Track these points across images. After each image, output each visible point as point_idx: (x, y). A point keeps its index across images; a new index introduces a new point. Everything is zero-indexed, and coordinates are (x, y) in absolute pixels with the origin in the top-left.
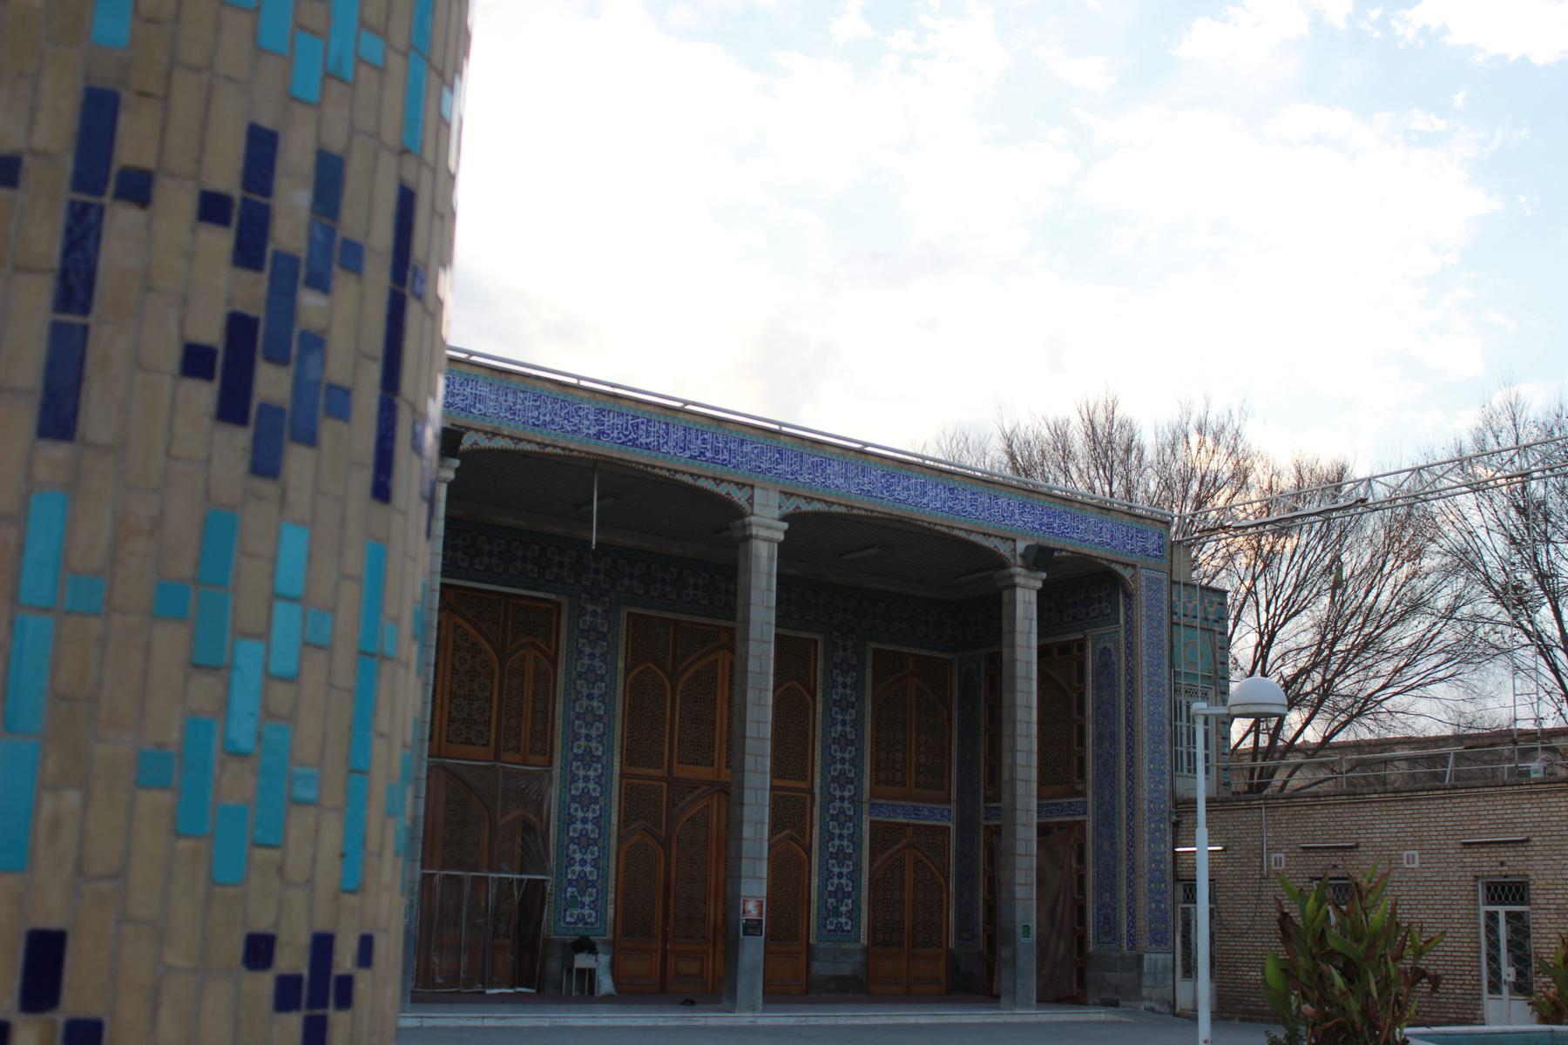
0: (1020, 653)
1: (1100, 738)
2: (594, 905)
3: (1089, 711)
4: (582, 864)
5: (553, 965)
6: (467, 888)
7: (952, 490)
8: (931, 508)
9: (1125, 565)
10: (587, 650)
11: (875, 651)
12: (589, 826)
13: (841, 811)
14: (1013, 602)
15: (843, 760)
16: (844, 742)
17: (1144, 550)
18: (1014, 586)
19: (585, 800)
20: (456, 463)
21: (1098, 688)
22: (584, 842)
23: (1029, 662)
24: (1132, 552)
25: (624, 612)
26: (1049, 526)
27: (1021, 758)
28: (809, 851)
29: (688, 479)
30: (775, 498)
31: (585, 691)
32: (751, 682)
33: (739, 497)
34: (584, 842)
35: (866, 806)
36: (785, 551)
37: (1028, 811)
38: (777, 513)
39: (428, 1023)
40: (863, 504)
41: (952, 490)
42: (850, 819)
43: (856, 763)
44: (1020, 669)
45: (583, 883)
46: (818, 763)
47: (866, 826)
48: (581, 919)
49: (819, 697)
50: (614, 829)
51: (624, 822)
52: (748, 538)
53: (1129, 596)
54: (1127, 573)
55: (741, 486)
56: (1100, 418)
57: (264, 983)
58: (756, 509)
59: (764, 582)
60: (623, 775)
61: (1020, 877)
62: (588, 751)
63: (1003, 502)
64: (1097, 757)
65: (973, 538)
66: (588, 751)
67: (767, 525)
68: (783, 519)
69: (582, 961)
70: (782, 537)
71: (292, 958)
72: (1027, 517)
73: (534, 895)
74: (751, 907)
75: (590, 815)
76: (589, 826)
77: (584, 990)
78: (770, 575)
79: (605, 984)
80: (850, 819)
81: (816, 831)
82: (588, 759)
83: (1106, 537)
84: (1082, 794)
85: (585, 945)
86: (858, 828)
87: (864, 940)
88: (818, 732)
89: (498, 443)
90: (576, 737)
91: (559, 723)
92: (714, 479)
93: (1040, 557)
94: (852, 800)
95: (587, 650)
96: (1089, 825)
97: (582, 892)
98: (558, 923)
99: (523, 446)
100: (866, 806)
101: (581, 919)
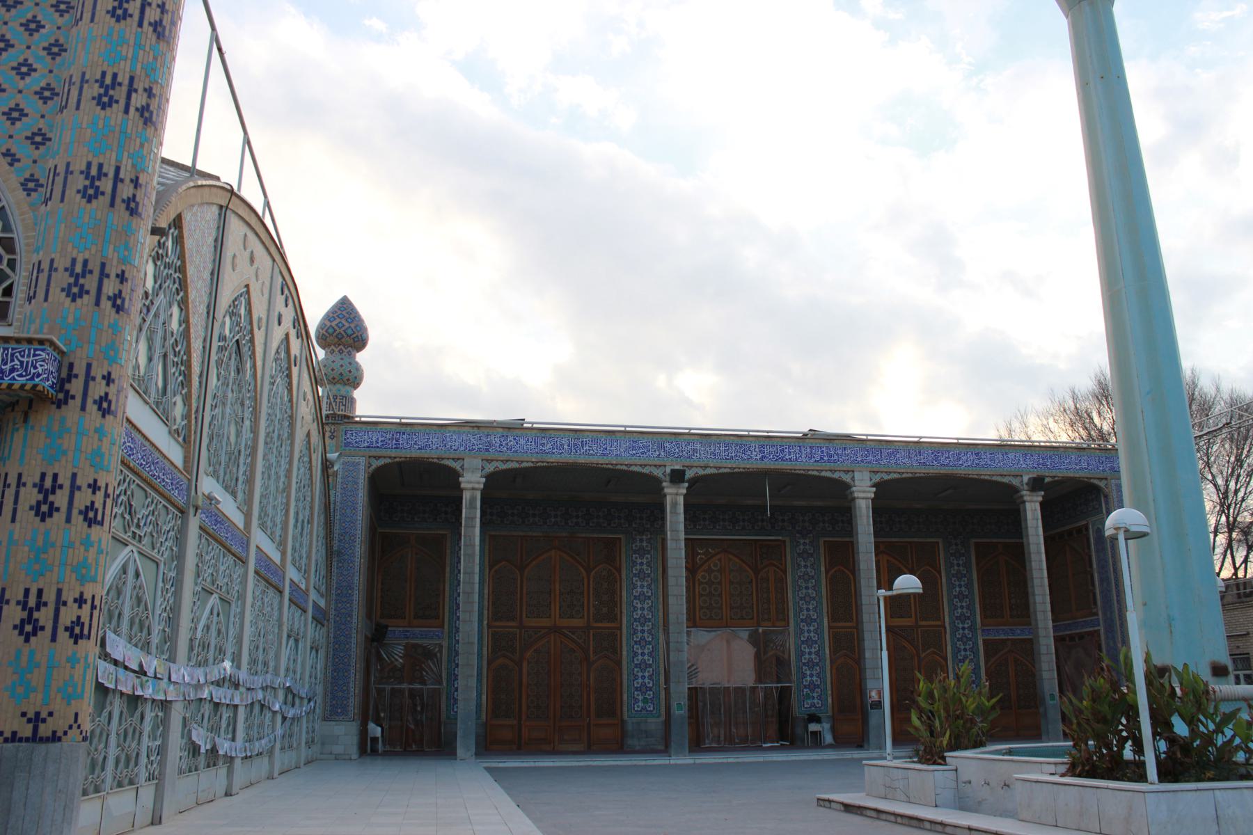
0: (1032, 539)
1: (1101, 580)
2: (820, 697)
3: (1095, 566)
4: (811, 676)
5: (799, 731)
6: (748, 693)
7: (977, 454)
8: (965, 467)
9: (1100, 479)
10: (803, 563)
11: (977, 544)
13: (964, 635)
14: (1025, 510)
15: (962, 607)
16: (961, 597)
18: (1024, 502)
19: (809, 642)
20: (686, 485)
21: (1097, 551)
22: (811, 665)
23: (1038, 544)
24: (1104, 470)
25: (822, 541)
26: (1044, 464)
27: (1038, 599)
28: (946, 659)
29: (815, 473)
30: (867, 475)
31: (804, 585)
32: (862, 575)
33: (846, 478)
34: (811, 665)
35: (979, 632)
37: (1046, 628)
38: (869, 483)
39: (698, 761)
40: (921, 471)
41: (977, 454)
42: (970, 639)
43: (970, 607)
44: (1033, 548)
45: (813, 687)
46: (946, 610)
47: (980, 642)
48: (813, 705)
49: (943, 574)
50: (828, 656)
51: (834, 651)
52: (854, 499)
53: (1106, 496)
54: (1102, 484)
55: (847, 472)
57: (25, 719)
58: (857, 483)
60: (830, 627)
61: (1045, 666)
62: (809, 616)
63: (1011, 456)
64: (1101, 592)
65: (994, 478)
66: (809, 616)
67: (472, 481)
69: (813, 727)
71: (31, 715)
72: (1028, 461)
73: (784, 694)
77: (816, 741)
79: (829, 738)
80: (970, 639)
81: (949, 648)
82: (809, 620)
83: (1084, 465)
84: (1096, 614)
85: (814, 718)
86: (975, 644)
88: (945, 593)
89: (708, 471)
90: (801, 610)
91: (791, 604)
93: (1037, 484)
94: (970, 629)
95: (803, 563)
96: (1102, 631)
97: (812, 691)
98: (800, 707)
99: (722, 471)
100: (979, 632)
101: (813, 705)
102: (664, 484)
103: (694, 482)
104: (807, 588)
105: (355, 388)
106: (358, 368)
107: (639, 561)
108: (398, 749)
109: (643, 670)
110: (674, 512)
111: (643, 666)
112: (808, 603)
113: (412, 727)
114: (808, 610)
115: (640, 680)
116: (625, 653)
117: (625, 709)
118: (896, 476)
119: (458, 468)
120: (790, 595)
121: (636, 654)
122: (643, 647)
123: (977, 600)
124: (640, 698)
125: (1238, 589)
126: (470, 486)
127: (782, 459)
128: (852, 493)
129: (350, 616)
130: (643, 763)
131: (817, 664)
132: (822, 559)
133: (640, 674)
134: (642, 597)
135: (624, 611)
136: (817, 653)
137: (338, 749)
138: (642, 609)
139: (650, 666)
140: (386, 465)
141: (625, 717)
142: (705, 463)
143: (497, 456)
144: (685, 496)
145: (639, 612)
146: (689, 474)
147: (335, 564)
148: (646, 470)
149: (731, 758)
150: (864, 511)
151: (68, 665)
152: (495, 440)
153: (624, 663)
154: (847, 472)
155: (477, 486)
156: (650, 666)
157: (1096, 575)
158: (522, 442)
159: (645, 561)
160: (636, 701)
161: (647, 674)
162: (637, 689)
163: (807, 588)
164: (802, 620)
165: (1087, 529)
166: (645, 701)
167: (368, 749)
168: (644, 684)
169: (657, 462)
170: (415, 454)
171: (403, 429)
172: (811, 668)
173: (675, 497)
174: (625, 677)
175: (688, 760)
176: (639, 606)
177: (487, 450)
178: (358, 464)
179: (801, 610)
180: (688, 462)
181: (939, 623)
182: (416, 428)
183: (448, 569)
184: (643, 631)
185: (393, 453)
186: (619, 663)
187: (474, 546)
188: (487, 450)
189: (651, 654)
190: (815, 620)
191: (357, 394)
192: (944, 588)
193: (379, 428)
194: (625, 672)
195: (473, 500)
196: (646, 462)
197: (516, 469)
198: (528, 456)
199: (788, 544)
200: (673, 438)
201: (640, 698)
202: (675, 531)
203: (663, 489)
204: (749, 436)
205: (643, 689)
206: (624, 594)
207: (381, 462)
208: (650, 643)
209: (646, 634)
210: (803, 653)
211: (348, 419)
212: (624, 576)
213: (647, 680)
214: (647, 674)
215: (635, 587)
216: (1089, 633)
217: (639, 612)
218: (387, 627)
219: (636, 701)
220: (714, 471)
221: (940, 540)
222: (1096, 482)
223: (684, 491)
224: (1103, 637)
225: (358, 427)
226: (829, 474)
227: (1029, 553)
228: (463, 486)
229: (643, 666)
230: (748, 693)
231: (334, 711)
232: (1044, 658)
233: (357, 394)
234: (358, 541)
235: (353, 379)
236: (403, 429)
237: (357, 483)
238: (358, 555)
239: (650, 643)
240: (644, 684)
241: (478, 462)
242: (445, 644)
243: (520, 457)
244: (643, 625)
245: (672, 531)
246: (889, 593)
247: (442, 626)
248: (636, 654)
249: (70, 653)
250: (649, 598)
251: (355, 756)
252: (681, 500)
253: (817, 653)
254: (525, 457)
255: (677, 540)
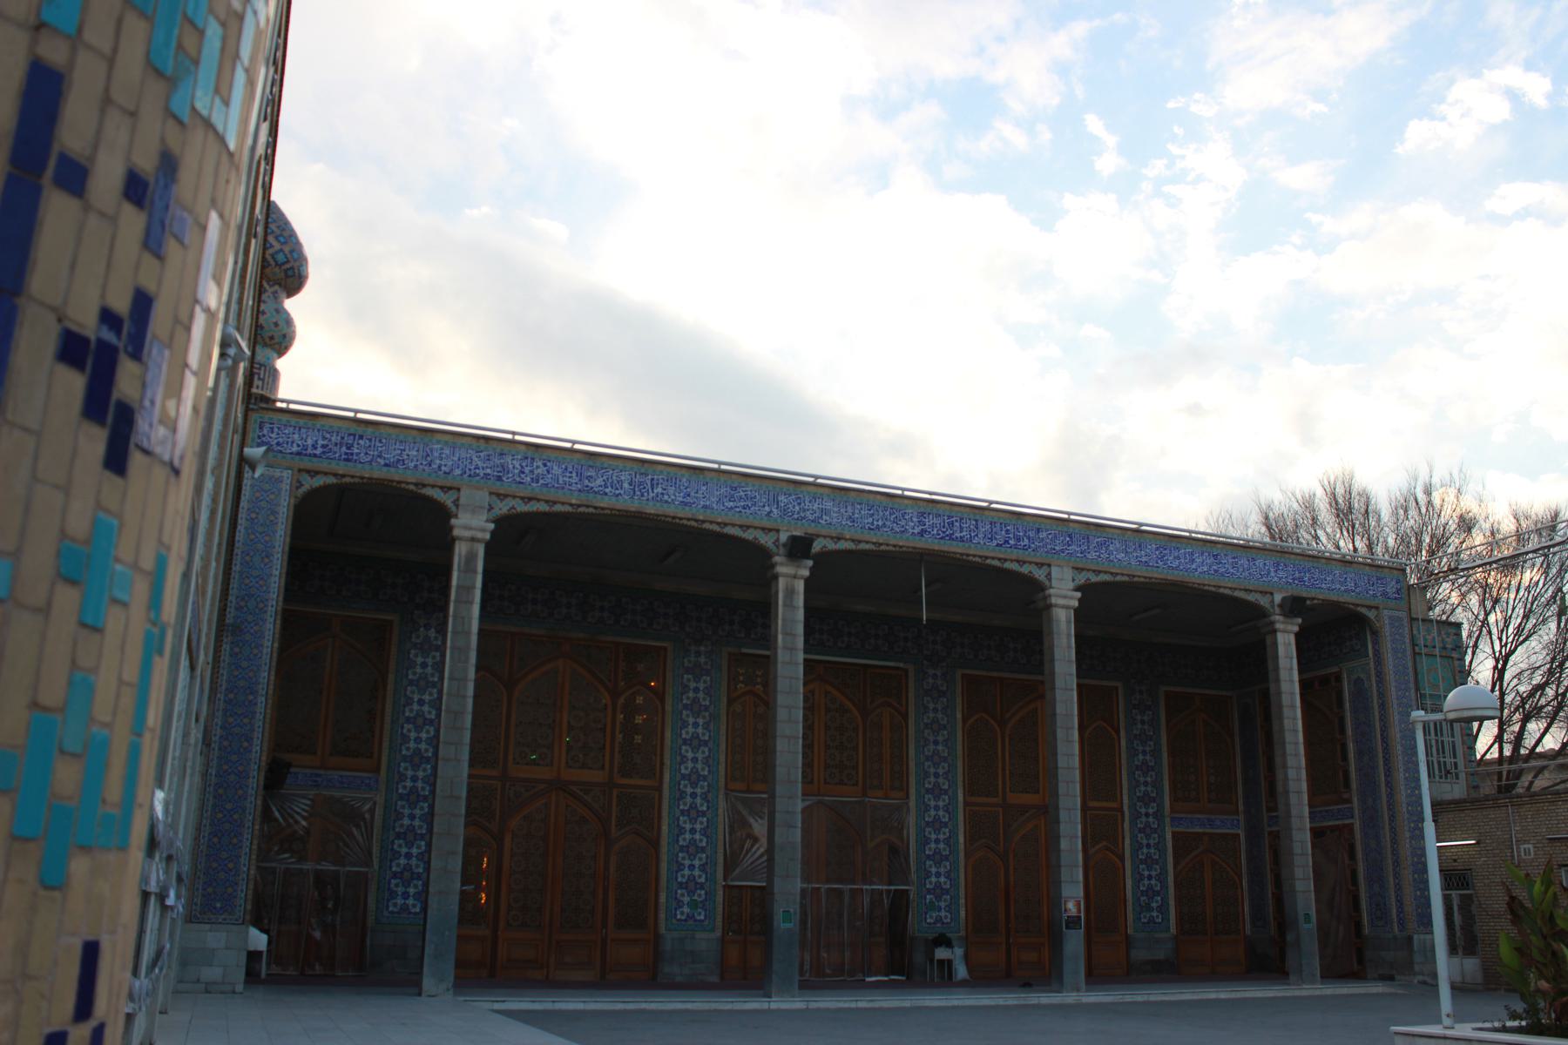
0: (1284, 687)
3: (1349, 732)
6: (847, 900)
7: (1215, 557)
9: (1370, 607)
10: (931, 706)
12: (942, 846)
14: (1275, 644)
17: (1384, 594)
18: (1275, 631)
19: (937, 824)
20: (810, 563)
22: (938, 858)
24: (1374, 596)
26: (1301, 580)
27: (1292, 774)
28: (1122, 859)
29: (996, 563)
30: (1068, 573)
34: (938, 858)
35: (1167, 820)
36: (1081, 615)
38: (1071, 585)
39: (813, 1005)
40: (1142, 572)
42: (1155, 831)
44: (1285, 700)
45: (939, 891)
47: (1169, 836)
49: (1122, 733)
50: (962, 847)
51: (971, 839)
52: (1049, 606)
53: (1375, 633)
54: (1371, 615)
55: (1040, 565)
56: (1340, 491)
58: (1054, 583)
59: (1064, 641)
60: (966, 804)
61: (1299, 873)
63: (1260, 563)
67: (472, 526)
68: (1077, 589)
69: (941, 953)
70: (1076, 604)
72: (1281, 574)
73: (900, 903)
74: (1071, 906)
75: (941, 837)
76: (942, 846)
77: (944, 977)
78: (1069, 635)
79: (961, 972)
80: (1155, 831)
81: (1127, 841)
82: (937, 792)
83: (1351, 585)
84: (1349, 801)
85: (943, 941)
86: (1162, 837)
87: (1173, 930)
88: (1124, 762)
89: (842, 545)
90: (927, 775)
91: (912, 765)
92: (741, 526)
95: (931, 706)
96: (1357, 827)
97: (939, 898)
98: (921, 923)
100: (1167, 820)
102: (777, 559)
103: (823, 559)
104: (936, 743)
105: (281, 353)
106: (289, 322)
107: (693, 685)
108: (291, 972)
109: (692, 856)
110: (789, 604)
111: (692, 849)
112: (936, 765)
113: (317, 934)
114: (936, 775)
115: (686, 872)
116: (665, 828)
117: (662, 916)
118: (1107, 578)
119: (449, 503)
120: (912, 752)
121: (682, 831)
122: (693, 821)
123: (1166, 777)
124: (686, 899)
125: (1500, 779)
126: (467, 534)
127: (951, 537)
128: (1047, 597)
129: (250, 740)
130: (729, 1007)
131: (946, 858)
132: (959, 700)
133: (687, 862)
134: (695, 742)
135: (667, 762)
136: (947, 841)
137: (211, 973)
138: (695, 760)
139: (703, 850)
140: (325, 487)
141: (662, 930)
142: (838, 531)
143: (514, 489)
144: (807, 581)
145: (690, 765)
146: (817, 546)
147: (226, 647)
148: (749, 535)
149: (863, 1001)
150: (1063, 626)
151: (67, 598)
152: (513, 463)
153: (664, 842)
154: (1040, 565)
155: (479, 535)
156: (703, 850)
157: (1351, 746)
158: (556, 470)
159: (701, 686)
160: (680, 904)
161: (697, 863)
162: (681, 885)
163: (936, 743)
164: (928, 791)
165: (1338, 678)
166: (693, 905)
167: (258, 974)
168: (692, 878)
169: (766, 523)
170: (378, 472)
171: (360, 430)
172: (938, 864)
173: (792, 580)
174: (664, 866)
175: (797, 1004)
176: (690, 755)
177: (499, 478)
178: (279, 480)
179: (927, 775)
180: (812, 529)
181: (1113, 805)
182: (382, 430)
183: (391, 677)
184: (694, 795)
185: (341, 468)
186: (655, 844)
187: (468, 633)
188: (499, 478)
189: (704, 832)
190: (946, 792)
191: (281, 364)
192: (1124, 756)
193: (319, 423)
194: (664, 857)
195: (471, 558)
196: (750, 520)
197: (545, 514)
198: (568, 495)
199: (911, 674)
200: (791, 487)
201: (686, 899)
202: (789, 634)
203: (773, 566)
204: (902, 497)
205: (691, 885)
206: (668, 734)
207: (319, 482)
208: (704, 814)
209: (698, 800)
210: (927, 841)
211: (267, 402)
212: (668, 708)
213: (696, 873)
214: (697, 863)
215: (685, 725)
216: (1345, 826)
217: (690, 765)
218: (289, 765)
219: (680, 904)
220: (850, 546)
221: (1119, 684)
222: (1363, 610)
223: (806, 573)
224: (1358, 835)
225: (285, 418)
226: (1014, 567)
227: (1280, 707)
228: (456, 532)
229: (692, 849)
230: (847, 900)
231: (207, 903)
232: (1298, 861)
233: (281, 364)
234: (271, 610)
235: (276, 337)
236: (360, 430)
237: (274, 513)
238: (268, 635)
239: (704, 814)
240: (692, 878)
241: (483, 497)
242: (380, 799)
243: (552, 495)
244: (694, 785)
245: (785, 634)
246: (1438, 716)
247: (377, 770)
248: (682, 831)
249: (78, 524)
250: (706, 743)
251: (240, 988)
252: (800, 586)
253: (947, 841)
254: (560, 496)
255: (792, 649)
